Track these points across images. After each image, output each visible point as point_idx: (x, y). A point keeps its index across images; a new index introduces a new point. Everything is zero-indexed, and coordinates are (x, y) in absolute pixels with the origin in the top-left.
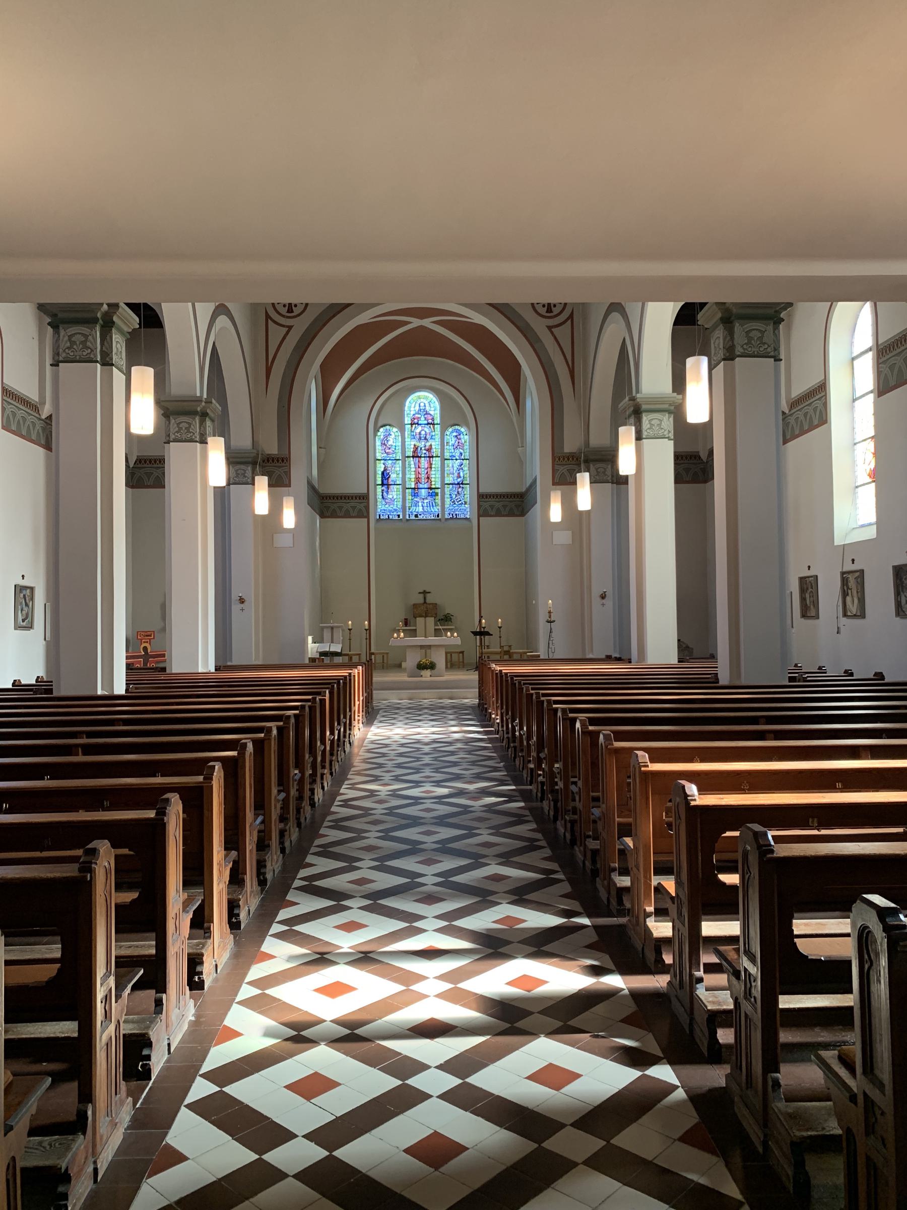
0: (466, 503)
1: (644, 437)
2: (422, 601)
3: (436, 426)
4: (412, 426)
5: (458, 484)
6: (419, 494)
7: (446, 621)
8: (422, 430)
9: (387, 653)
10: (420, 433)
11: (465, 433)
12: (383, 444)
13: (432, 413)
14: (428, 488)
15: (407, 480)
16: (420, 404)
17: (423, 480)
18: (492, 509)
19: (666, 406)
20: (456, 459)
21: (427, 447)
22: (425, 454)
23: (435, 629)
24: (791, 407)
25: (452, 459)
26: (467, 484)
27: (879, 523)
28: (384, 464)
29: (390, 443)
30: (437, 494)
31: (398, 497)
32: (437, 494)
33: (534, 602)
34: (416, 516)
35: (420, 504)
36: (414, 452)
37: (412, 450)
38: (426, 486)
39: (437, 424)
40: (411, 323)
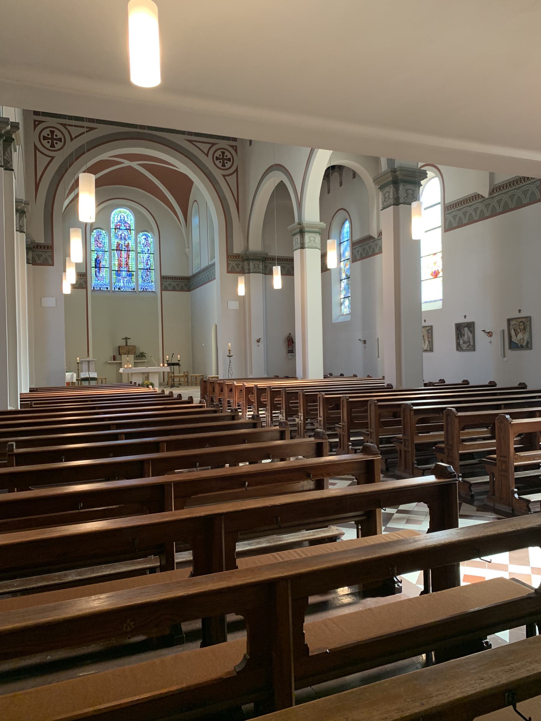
0: (152, 282)
1: (306, 247)
2: (124, 344)
3: (132, 231)
4: (115, 230)
5: (147, 269)
6: (121, 274)
7: (142, 357)
8: (122, 233)
9: (106, 379)
10: (121, 235)
11: (151, 237)
12: (96, 241)
13: (129, 222)
14: (127, 271)
15: (112, 265)
16: (121, 216)
17: (123, 266)
18: (170, 286)
19: (318, 230)
20: (145, 253)
21: (126, 244)
22: (125, 248)
23: (134, 362)
24: (380, 235)
25: (142, 253)
26: (153, 270)
27: (444, 300)
28: (96, 254)
29: (100, 240)
30: (133, 275)
31: (107, 275)
32: (133, 275)
33: (203, 344)
34: (119, 289)
35: (122, 281)
36: (117, 247)
37: (116, 245)
38: (125, 269)
39: (133, 230)
40: (123, 163)
